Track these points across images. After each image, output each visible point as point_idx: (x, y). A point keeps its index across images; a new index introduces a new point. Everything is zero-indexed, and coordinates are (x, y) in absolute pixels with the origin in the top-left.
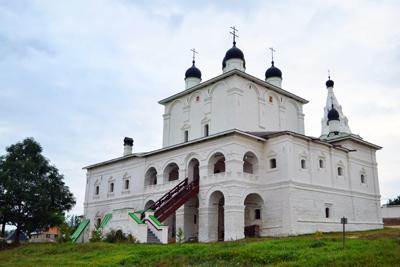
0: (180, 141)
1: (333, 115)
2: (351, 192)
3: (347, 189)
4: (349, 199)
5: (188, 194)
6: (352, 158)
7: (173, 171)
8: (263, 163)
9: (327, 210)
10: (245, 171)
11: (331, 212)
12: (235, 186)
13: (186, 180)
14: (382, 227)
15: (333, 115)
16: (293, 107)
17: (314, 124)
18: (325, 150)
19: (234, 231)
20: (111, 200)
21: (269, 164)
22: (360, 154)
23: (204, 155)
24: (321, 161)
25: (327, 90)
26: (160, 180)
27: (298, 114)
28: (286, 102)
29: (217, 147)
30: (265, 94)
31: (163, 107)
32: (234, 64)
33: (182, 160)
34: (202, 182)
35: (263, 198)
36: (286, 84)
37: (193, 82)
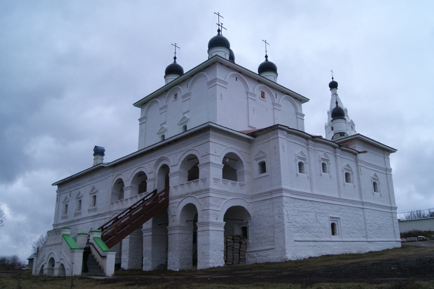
0: (156, 140)
1: (338, 113)
2: (363, 203)
3: (357, 199)
4: (361, 212)
5: (156, 208)
6: (362, 162)
7: (141, 180)
8: (249, 168)
9: (333, 225)
10: (223, 178)
11: (337, 228)
12: (217, 197)
13: (155, 191)
14: (399, 245)
15: (338, 113)
16: (289, 103)
17: (315, 121)
18: (329, 151)
19: (213, 253)
20: (78, 220)
21: (257, 168)
22: (369, 157)
23: (175, 159)
24: (324, 165)
25: (330, 92)
26: (127, 194)
27: (297, 114)
28: (281, 99)
29: (189, 147)
30: (256, 89)
31: (139, 109)
32: (222, 53)
33: (150, 168)
34: (173, 192)
35: (250, 212)
36: (283, 79)
37: (173, 78)
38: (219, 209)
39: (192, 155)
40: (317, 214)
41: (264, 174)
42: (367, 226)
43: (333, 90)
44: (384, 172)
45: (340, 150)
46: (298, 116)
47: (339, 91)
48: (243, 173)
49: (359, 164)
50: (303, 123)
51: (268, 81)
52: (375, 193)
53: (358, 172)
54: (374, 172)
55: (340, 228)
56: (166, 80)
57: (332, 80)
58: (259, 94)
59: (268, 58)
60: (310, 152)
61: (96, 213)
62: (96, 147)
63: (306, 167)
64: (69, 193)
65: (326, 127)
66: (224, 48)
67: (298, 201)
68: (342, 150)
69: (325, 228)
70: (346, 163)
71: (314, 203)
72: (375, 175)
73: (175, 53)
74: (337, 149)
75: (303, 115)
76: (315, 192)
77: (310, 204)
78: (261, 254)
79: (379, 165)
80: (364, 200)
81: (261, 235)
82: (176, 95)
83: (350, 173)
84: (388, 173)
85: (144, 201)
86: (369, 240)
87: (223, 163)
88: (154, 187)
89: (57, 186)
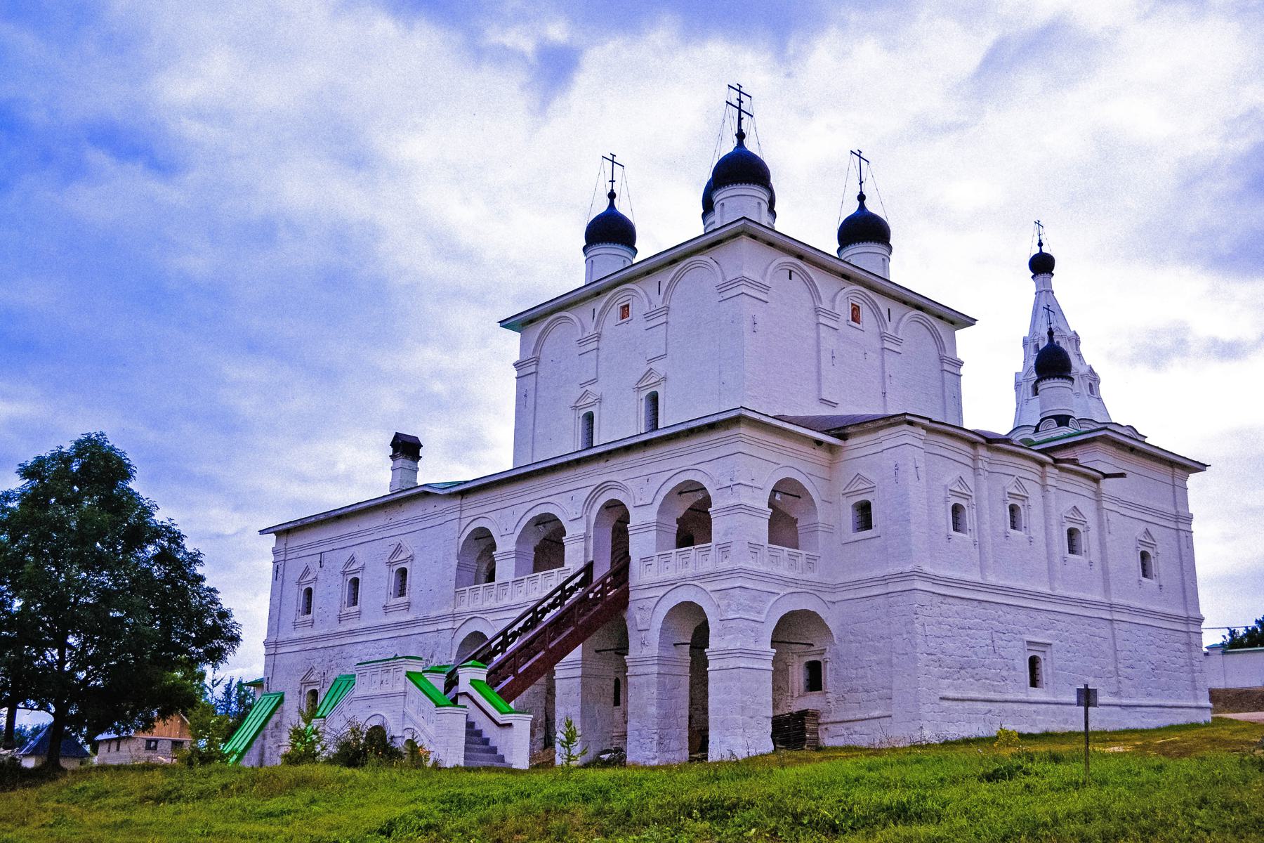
1: (1052, 361)
4: (1105, 631)
5: (596, 611)
9: (1033, 663)
11: (1045, 669)
15: (1052, 361)
17: (991, 394)
18: (1029, 471)
20: (351, 633)
21: (848, 517)
23: (645, 489)
24: (1013, 509)
26: (505, 569)
29: (687, 462)
30: (837, 296)
31: (514, 338)
33: (572, 503)
34: (639, 575)
36: (906, 267)
37: (611, 259)
38: (762, 618)
39: (692, 483)
40: (995, 635)
41: (867, 533)
42: (1120, 666)
43: (1040, 277)
44: (1172, 525)
45: (1056, 471)
46: (946, 367)
47: (1059, 281)
48: (813, 528)
49: (1105, 505)
50: (958, 385)
51: (870, 276)
52: (1144, 579)
53: (1100, 525)
54: (1143, 526)
55: (1050, 671)
56: (590, 262)
57: (1037, 251)
58: (846, 314)
59: (866, 202)
60: (982, 478)
61: (409, 617)
62: (397, 436)
63: (969, 517)
64: (318, 558)
65: (1018, 385)
66: (756, 187)
67: (950, 600)
68: (1062, 470)
69: (1015, 669)
70: (1068, 503)
71: (987, 605)
72: (1147, 532)
73: (612, 181)
74: (1049, 469)
75: (959, 364)
76: (992, 579)
77: (980, 610)
78: (857, 728)
79: (1156, 505)
80: (1115, 600)
81: (860, 682)
82: (625, 310)
83: (1080, 528)
84: (1181, 526)
85: (564, 591)
86: (1125, 701)
87: (770, 505)
88: (586, 556)
89: (273, 536)
